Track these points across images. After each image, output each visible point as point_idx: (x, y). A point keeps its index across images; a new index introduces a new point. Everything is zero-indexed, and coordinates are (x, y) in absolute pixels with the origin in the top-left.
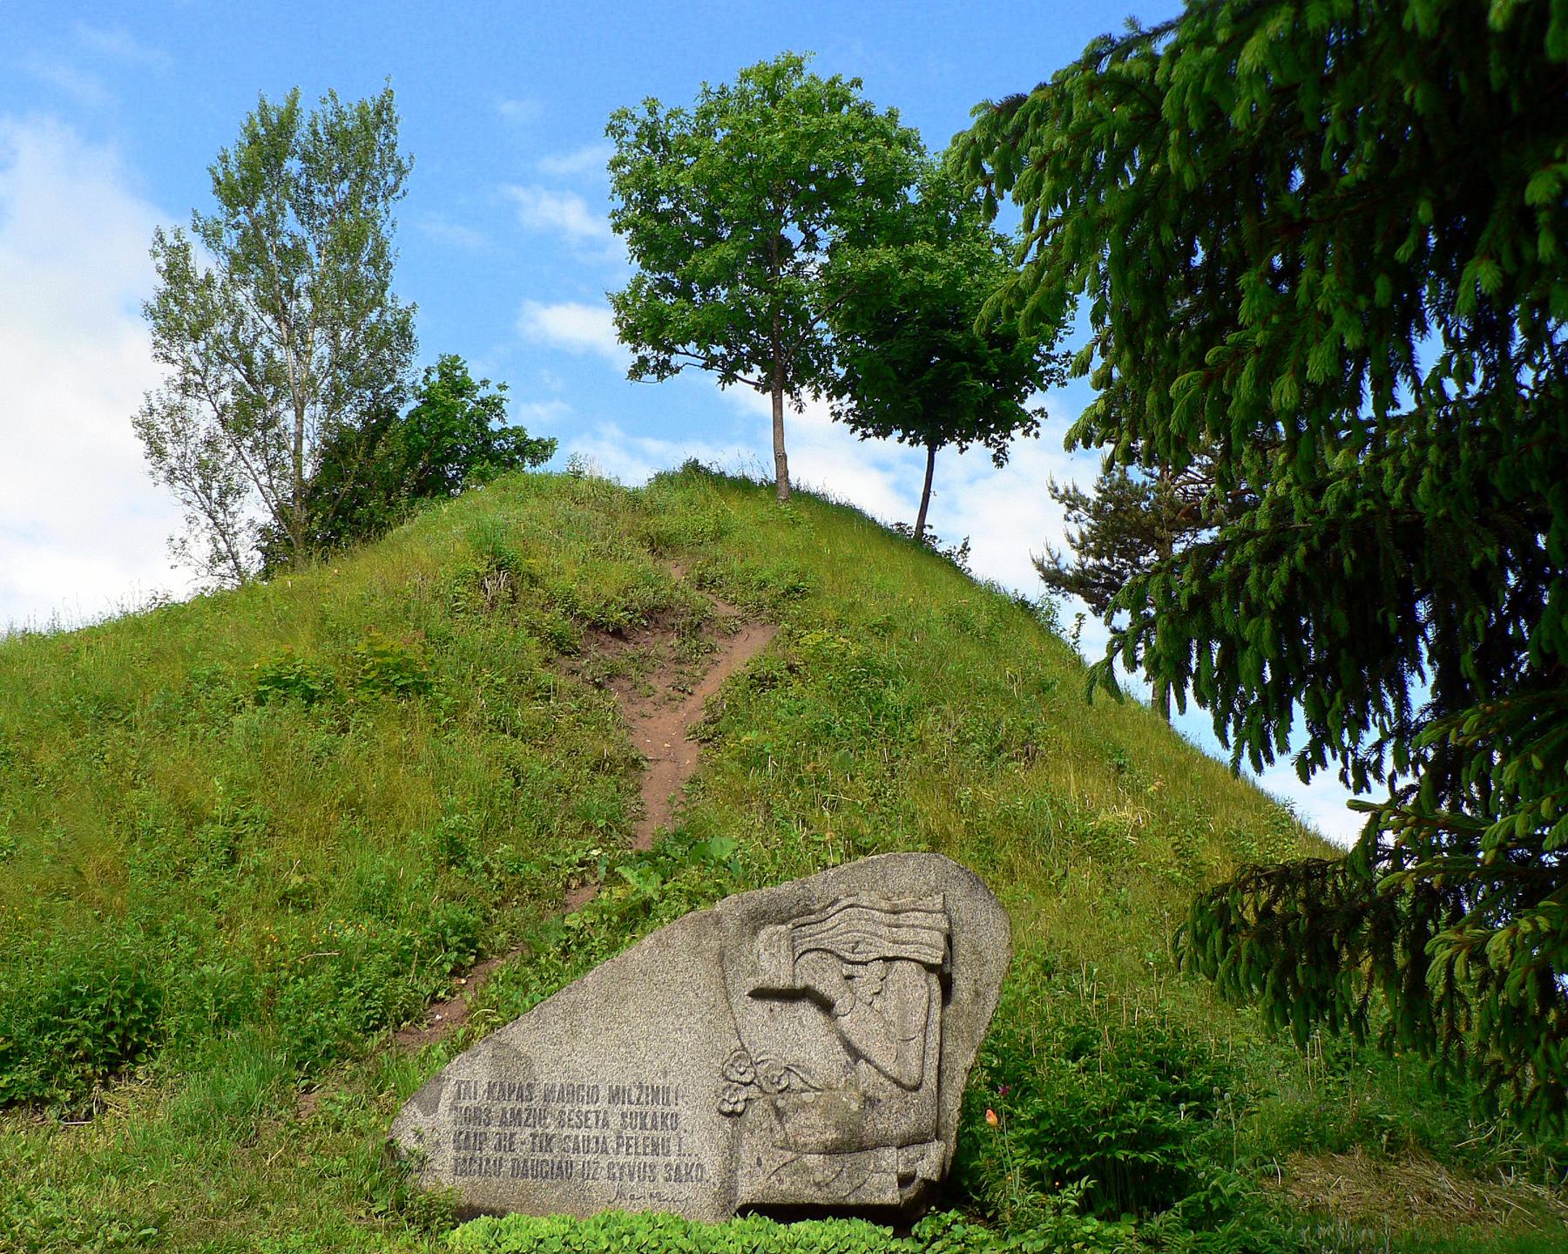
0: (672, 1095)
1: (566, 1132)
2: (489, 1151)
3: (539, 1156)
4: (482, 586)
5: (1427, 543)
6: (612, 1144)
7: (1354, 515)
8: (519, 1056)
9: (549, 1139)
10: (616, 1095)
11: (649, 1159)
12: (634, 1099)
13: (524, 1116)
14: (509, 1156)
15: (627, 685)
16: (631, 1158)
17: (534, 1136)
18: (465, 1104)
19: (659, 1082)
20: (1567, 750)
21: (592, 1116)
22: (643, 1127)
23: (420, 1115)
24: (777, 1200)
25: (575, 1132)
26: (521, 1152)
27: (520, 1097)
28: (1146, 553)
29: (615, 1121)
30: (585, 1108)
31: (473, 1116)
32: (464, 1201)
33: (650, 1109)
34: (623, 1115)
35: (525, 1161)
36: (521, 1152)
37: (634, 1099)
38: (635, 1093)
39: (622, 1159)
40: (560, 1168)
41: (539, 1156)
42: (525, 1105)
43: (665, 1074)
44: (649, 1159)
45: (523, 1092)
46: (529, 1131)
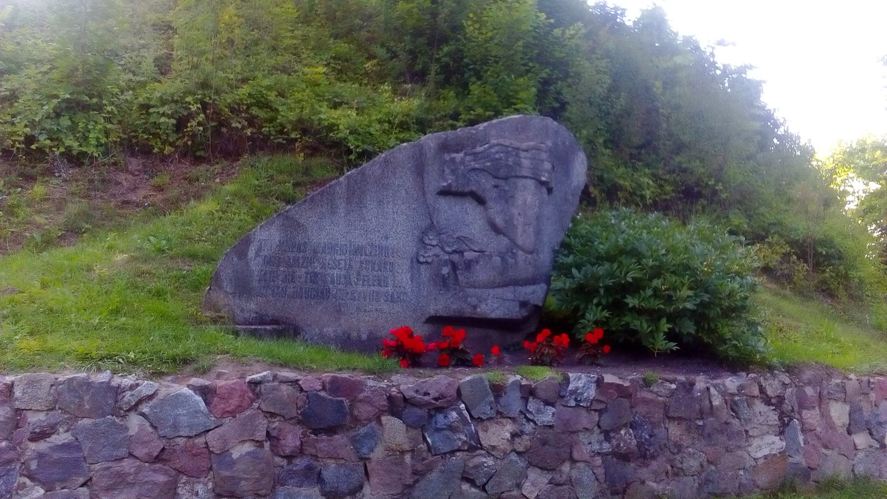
4: (380, 148)
5: (47, 150)
9: (316, 275)
11: (376, 288)
15: (140, 452)
16: (365, 288)
17: (307, 273)
20: (2, 88)
21: (343, 262)
22: (373, 269)
24: (451, 314)
28: (237, 127)
30: (338, 257)
34: (361, 263)
35: (301, 289)
39: (360, 288)
40: (322, 293)
43: (387, 238)
44: (376, 288)
46: (304, 270)
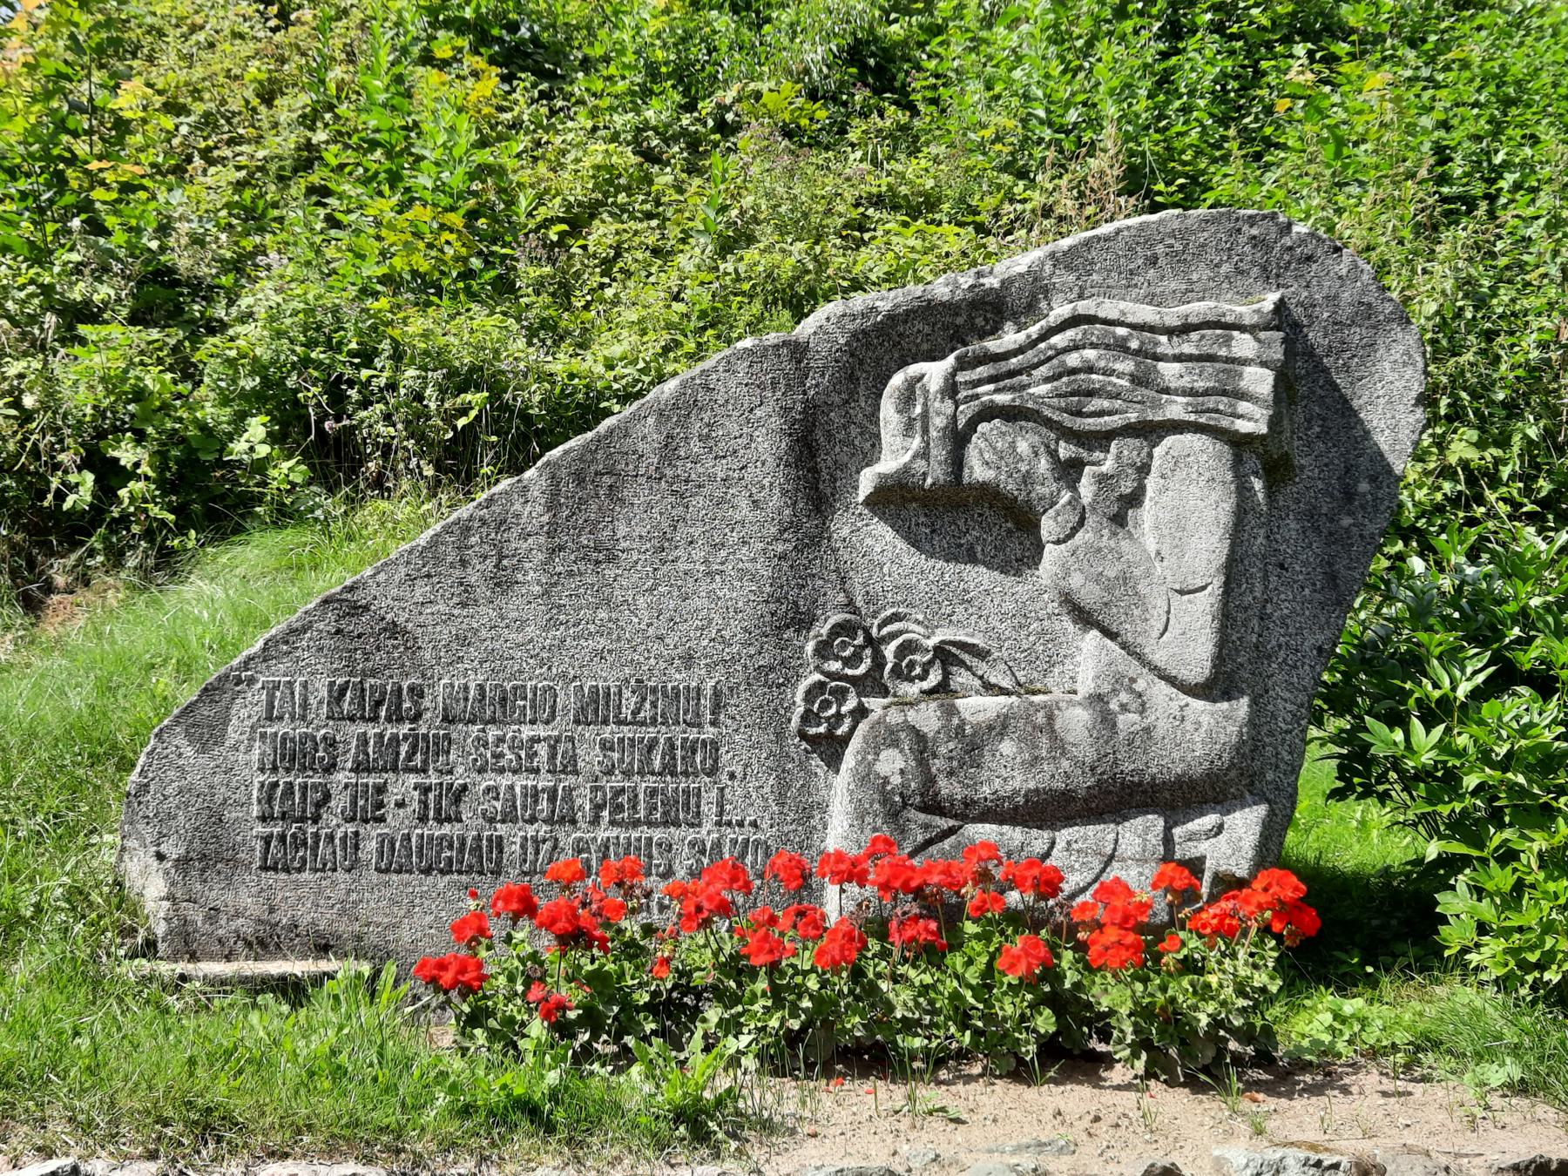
0: (706, 703)
1: (490, 780)
2: (332, 820)
3: (436, 830)
6: (584, 802)
7: (46, 504)
8: (394, 630)
10: (595, 708)
12: (626, 713)
13: (404, 748)
14: (373, 831)
18: (281, 728)
19: (678, 678)
21: (542, 750)
23: (189, 751)
25: (504, 781)
26: (398, 822)
27: (396, 717)
29: (590, 757)
30: (527, 732)
31: (292, 755)
32: (1522, 1103)
33: (662, 734)
36: (398, 822)
37: (626, 713)
38: (629, 701)
40: (477, 848)
41: (436, 830)
42: (405, 729)
45: (396, 705)
46: (413, 779)
